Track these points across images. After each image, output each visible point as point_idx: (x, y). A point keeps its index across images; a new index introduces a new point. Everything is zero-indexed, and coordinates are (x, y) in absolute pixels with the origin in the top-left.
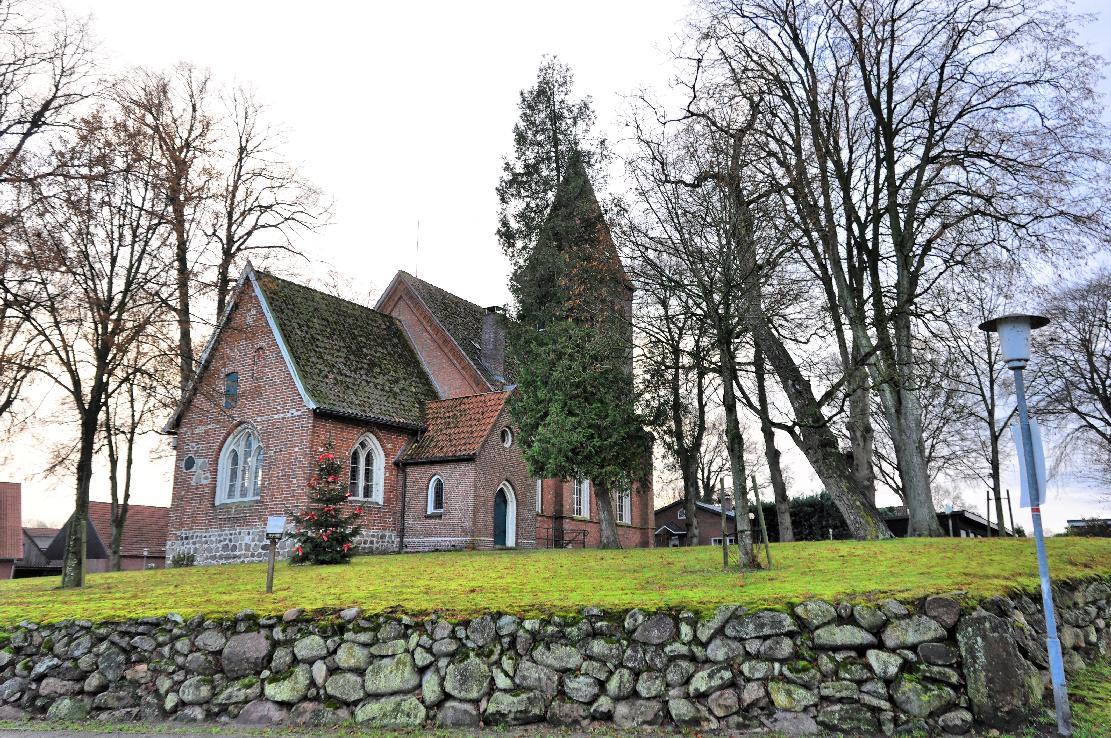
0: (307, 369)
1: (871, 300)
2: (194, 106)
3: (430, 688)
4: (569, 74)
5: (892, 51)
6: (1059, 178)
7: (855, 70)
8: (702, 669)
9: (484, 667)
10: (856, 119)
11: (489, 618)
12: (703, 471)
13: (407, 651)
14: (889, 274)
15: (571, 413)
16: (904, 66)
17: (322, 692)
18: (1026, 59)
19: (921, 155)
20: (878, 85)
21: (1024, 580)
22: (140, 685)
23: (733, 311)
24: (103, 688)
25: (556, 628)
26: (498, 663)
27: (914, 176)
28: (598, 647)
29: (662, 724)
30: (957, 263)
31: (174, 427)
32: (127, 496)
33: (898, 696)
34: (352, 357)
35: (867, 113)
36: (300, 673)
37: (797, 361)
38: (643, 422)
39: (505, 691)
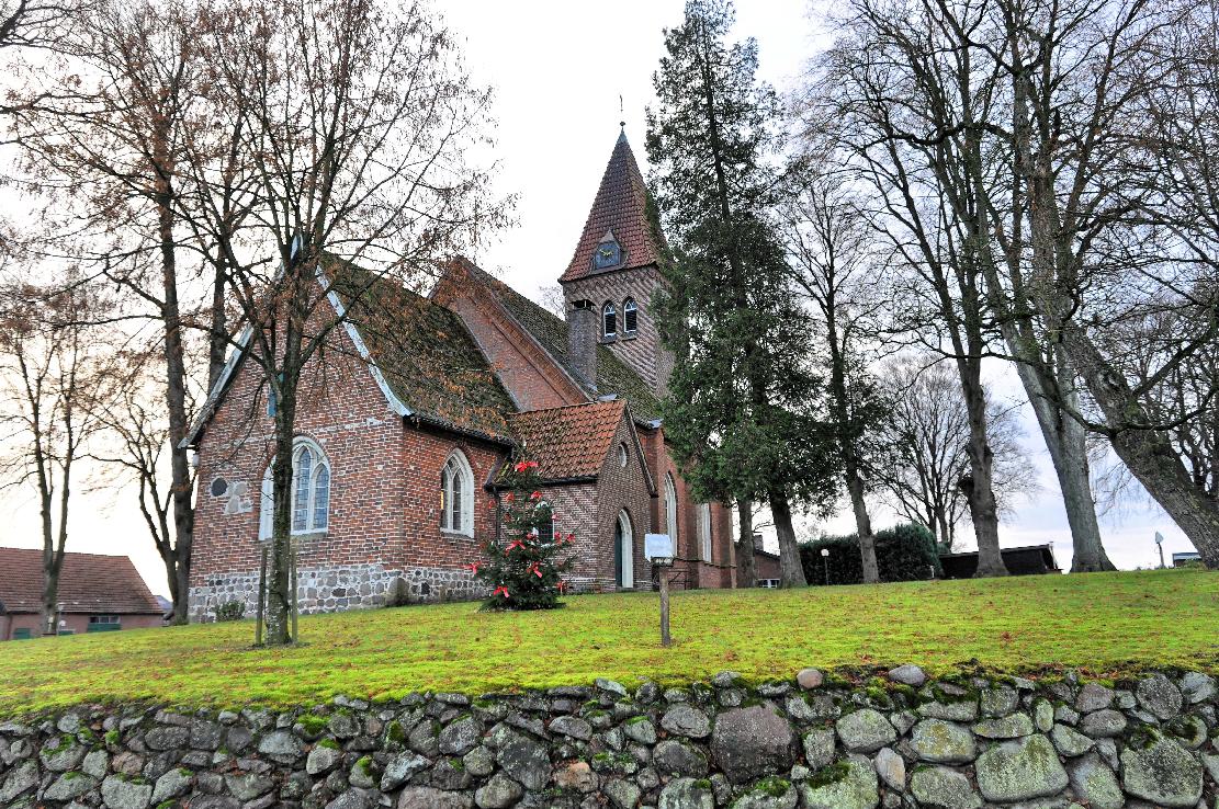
4: (730, 9)
32: (63, 536)
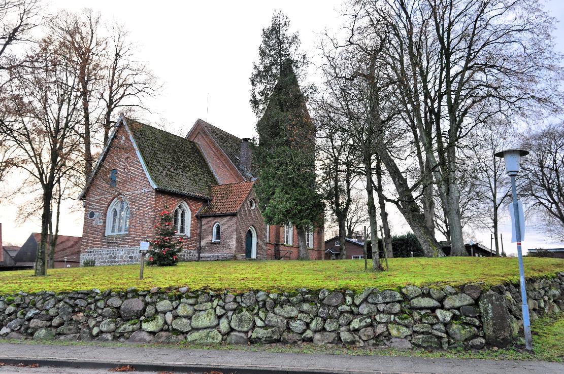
0: (152, 168)
1: (436, 139)
2: (92, 31)
3: (224, 325)
4: (288, 20)
5: (451, 12)
6: (532, 79)
7: (432, 22)
8: (356, 318)
9: (250, 316)
10: (431, 46)
11: (252, 293)
12: (348, 222)
13: (212, 308)
14: (445, 126)
15: (286, 193)
16: (456, 20)
17: (170, 327)
18: (518, 18)
19: (464, 66)
20: (443, 30)
21: (511, 277)
22: (80, 323)
23: (371, 147)
24: (61, 324)
25: (287, 297)
26: (257, 314)
27: (459, 77)
28: (306, 307)
29: (337, 344)
30: (481, 122)
31: (83, 197)
32: (57, 231)
33: (451, 331)
34: (175, 163)
35: (437, 44)
36: (160, 318)
37: (401, 169)
38: (322, 198)
39: (260, 327)
